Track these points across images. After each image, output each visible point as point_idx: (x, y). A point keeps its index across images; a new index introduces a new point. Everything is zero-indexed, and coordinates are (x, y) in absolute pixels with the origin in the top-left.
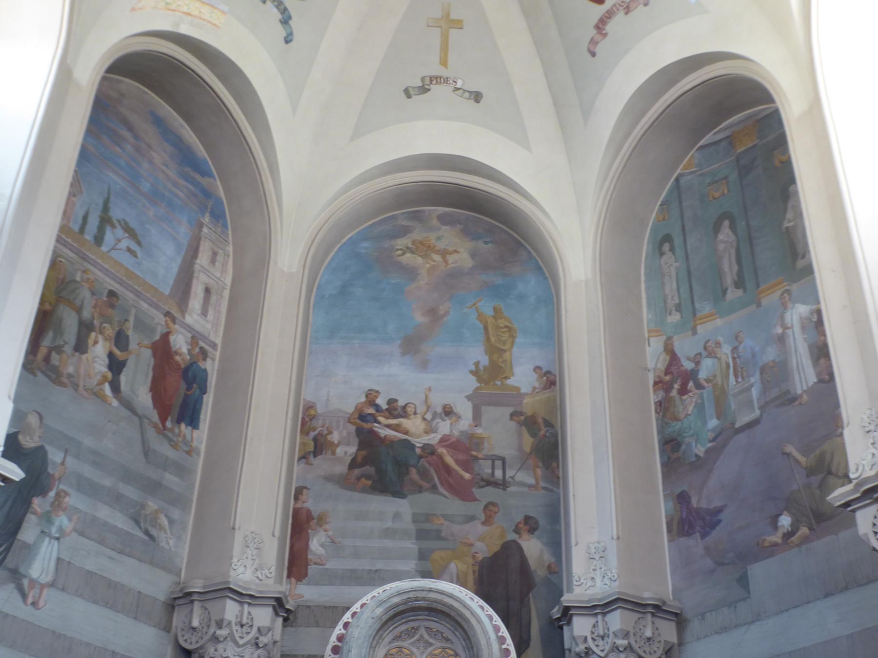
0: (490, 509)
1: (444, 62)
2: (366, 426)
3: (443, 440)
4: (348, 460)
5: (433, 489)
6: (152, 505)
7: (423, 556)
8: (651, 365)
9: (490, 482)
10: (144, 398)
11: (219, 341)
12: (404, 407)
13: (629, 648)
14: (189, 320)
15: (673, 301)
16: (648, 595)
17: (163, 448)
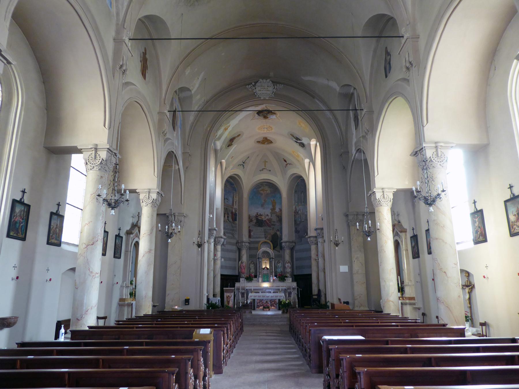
0: (273, 228)
1: (265, 166)
2: (257, 218)
3: (267, 219)
4: (255, 222)
6: (233, 232)
7: (265, 235)
8: (294, 209)
9: (273, 225)
10: (231, 220)
15: (296, 201)
16: (291, 241)
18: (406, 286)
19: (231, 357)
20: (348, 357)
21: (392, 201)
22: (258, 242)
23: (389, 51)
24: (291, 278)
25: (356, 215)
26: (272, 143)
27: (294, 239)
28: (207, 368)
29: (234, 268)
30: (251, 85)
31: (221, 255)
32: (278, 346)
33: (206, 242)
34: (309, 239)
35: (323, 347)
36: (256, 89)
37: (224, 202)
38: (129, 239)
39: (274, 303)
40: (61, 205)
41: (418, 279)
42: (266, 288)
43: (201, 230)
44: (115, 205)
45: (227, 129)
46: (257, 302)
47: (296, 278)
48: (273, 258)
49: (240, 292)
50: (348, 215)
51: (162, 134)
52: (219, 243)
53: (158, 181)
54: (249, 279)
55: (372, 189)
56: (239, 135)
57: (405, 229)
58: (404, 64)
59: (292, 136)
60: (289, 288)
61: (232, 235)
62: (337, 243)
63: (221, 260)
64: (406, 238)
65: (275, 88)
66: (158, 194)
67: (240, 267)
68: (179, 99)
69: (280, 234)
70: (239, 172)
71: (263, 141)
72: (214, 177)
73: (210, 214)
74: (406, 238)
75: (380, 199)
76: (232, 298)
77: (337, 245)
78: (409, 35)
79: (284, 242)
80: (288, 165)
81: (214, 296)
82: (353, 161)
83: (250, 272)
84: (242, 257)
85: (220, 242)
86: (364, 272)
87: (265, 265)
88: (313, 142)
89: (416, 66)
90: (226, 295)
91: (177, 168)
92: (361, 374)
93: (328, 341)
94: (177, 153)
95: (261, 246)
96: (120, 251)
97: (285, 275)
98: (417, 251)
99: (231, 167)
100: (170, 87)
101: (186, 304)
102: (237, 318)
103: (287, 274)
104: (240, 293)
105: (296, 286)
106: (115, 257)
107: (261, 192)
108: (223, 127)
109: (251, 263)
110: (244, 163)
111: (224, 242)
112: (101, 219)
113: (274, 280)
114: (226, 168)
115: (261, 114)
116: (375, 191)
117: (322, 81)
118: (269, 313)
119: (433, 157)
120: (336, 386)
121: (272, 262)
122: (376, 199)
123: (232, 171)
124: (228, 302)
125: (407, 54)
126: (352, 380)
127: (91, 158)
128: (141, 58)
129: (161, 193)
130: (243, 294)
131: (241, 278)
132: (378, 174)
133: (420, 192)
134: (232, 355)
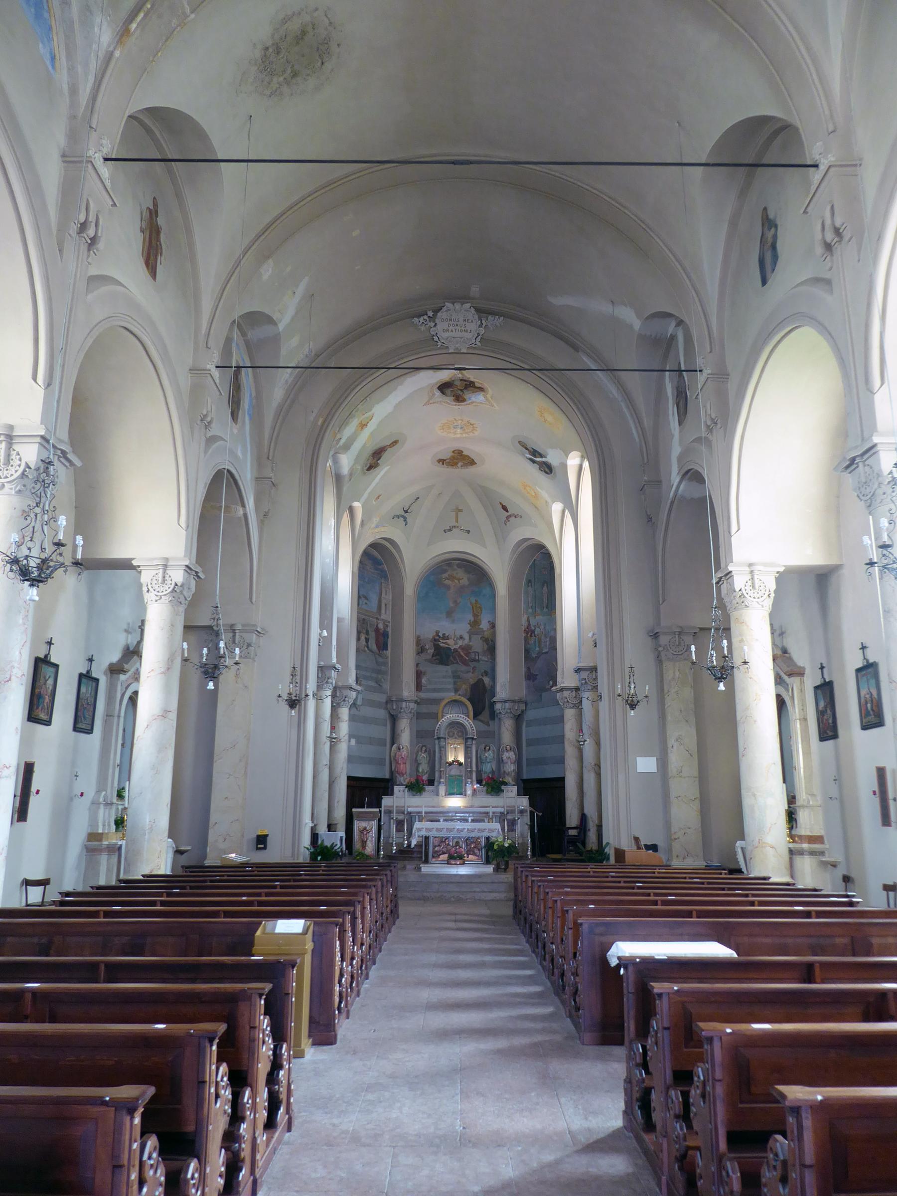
0: (474, 668)
1: (457, 521)
2: (436, 643)
3: (460, 647)
5: (457, 663)
6: (380, 676)
7: (455, 683)
9: (474, 660)
10: (374, 647)
11: (390, 620)
12: (448, 636)
13: (511, 712)
14: (382, 617)
16: (517, 698)
17: (380, 660)
18: (802, 810)
19: (362, 990)
20: (729, 1031)
21: (773, 595)
22: (436, 701)
23: (771, 216)
24: (516, 787)
25: (677, 634)
26: (474, 466)
27: (523, 693)
28: (286, 1041)
29: (381, 762)
30: (426, 317)
31: (350, 731)
32: (488, 958)
33: (311, 694)
34: (558, 695)
35: (625, 979)
36: (438, 327)
37: (358, 604)
38: (117, 684)
39: (474, 847)
40: (53, 644)
41: (834, 791)
42: (457, 811)
43: (298, 665)
44: (39, 575)
45: (366, 425)
46: (433, 843)
47: (527, 787)
48: (473, 739)
49: (393, 818)
50: (657, 633)
51: (199, 422)
52: (344, 700)
53: (189, 539)
54: (416, 787)
55: (723, 565)
56: (395, 443)
57: (801, 667)
58: (819, 236)
59: (523, 446)
60: (511, 811)
61: (376, 682)
62: (632, 701)
63: (349, 741)
64: (802, 691)
65: (483, 326)
66: (187, 572)
67: (393, 760)
68: (247, 344)
69: (491, 683)
70: (394, 532)
71: (453, 458)
72: (333, 542)
73: (321, 629)
74: (802, 691)
75: (743, 590)
76: (374, 833)
77: (633, 706)
78: (833, 159)
79: (501, 702)
80: (512, 519)
81: (331, 827)
82: (672, 503)
83: (417, 771)
84: (398, 735)
85: (346, 699)
86: (696, 774)
87: (456, 754)
88: (573, 460)
89: (854, 238)
90: (358, 825)
91: (241, 512)
92: (804, 1115)
93: (640, 962)
94: (240, 476)
95: (447, 709)
96: (91, 714)
97: (501, 779)
98: (830, 721)
99: (375, 520)
100: (220, 306)
101: (258, 849)
102: (383, 886)
103: (507, 777)
104: (392, 821)
105: (528, 805)
106: (76, 729)
107: (447, 582)
108: (356, 419)
109: (421, 749)
110: (406, 512)
111: (356, 700)
112: (21, 621)
113: (474, 791)
114: (362, 521)
115: (448, 391)
116: (731, 572)
117: (599, 306)
118: (463, 870)
119: (746, 590)
120: (677, 1112)
121: (471, 748)
122: (735, 591)
123: (378, 530)
124: (364, 843)
125: (828, 208)
126: (685, 1050)
127: (156, 582)
128: (144, 223)
129: (196, 568)
130: (400, 824)
131: (395, 787)
132: (739, 530)
133: (889, 546)
134: (366, 986)
